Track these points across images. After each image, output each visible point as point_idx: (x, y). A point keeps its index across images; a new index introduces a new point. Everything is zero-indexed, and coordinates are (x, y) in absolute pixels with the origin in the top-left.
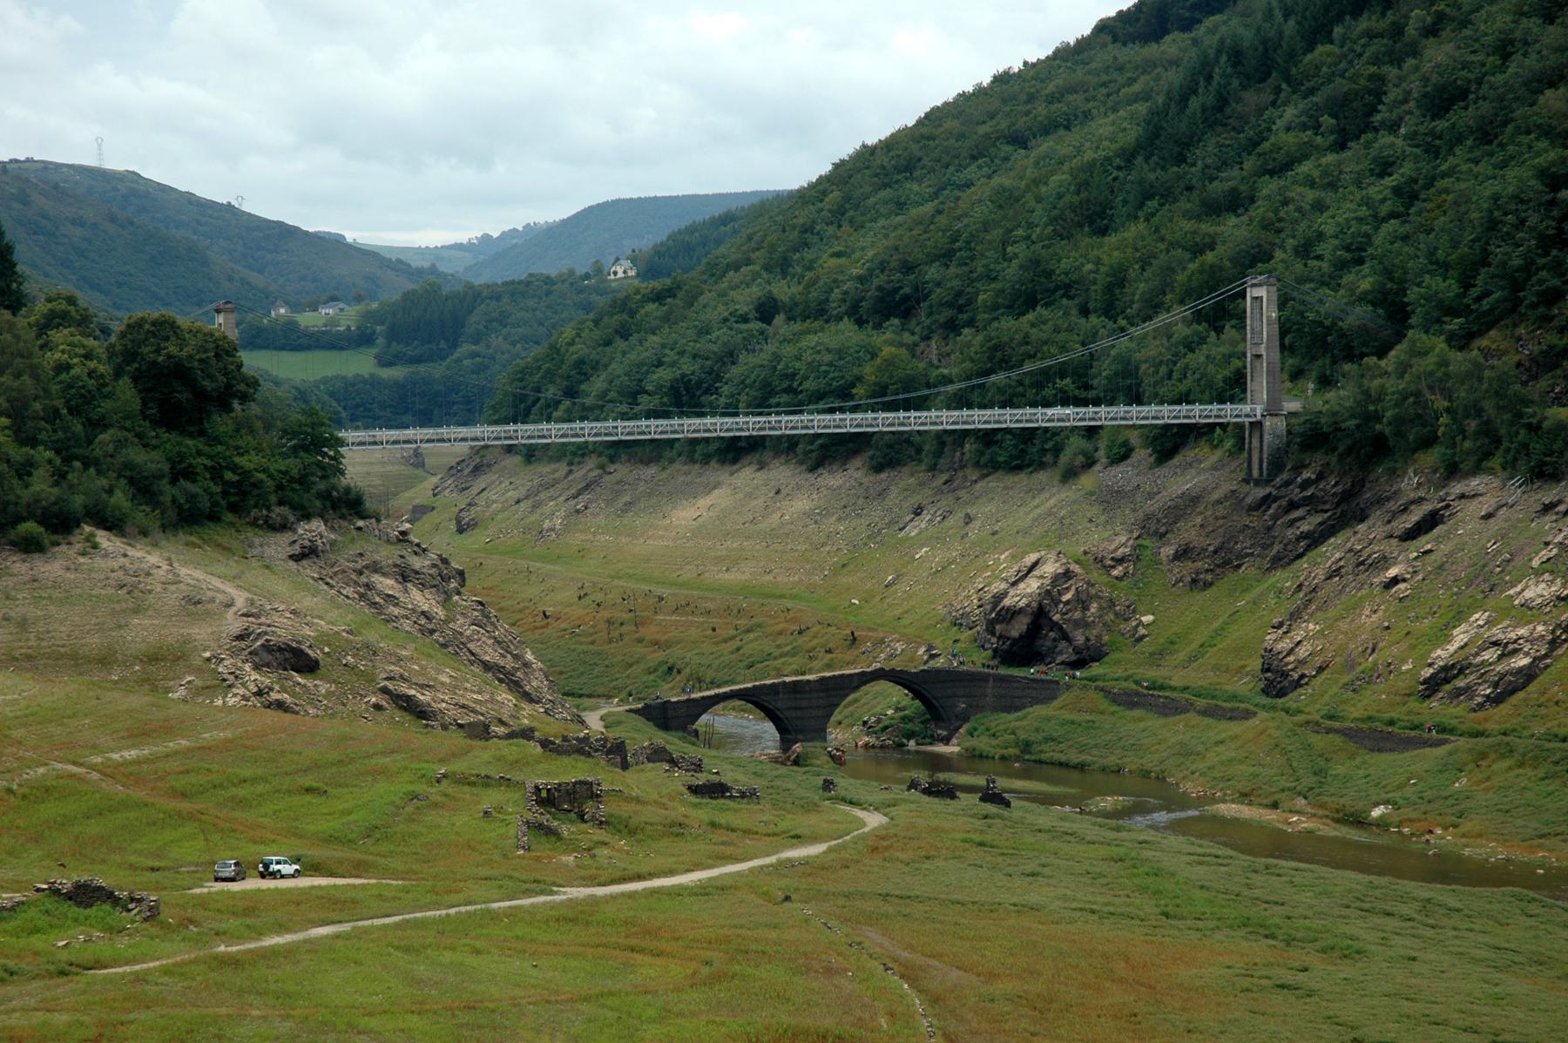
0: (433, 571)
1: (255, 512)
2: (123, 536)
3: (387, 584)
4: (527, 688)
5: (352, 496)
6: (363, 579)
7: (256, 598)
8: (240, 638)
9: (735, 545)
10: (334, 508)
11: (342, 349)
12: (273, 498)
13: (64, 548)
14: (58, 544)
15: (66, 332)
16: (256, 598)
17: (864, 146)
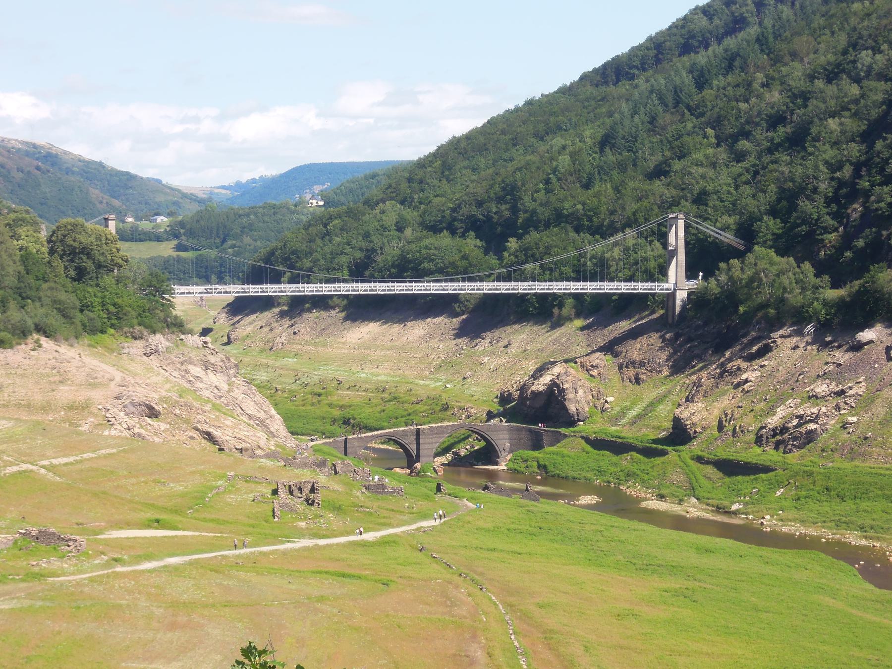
0: (221, 364)
1: (126, 329)
2: (56, 341)
3: (197, 370)
4: (272, 429)
5: (178, 321)
6: (184, 367)
7: (126, 376)
8: (117, 398)
9: (382, 353)
10: (168, 326)
11: (141, 240)
12: (135, 321)
13: (23, 346)
14: (20, 344)
15: (25, 229)
16: (126, 376)
17: (454, 137)
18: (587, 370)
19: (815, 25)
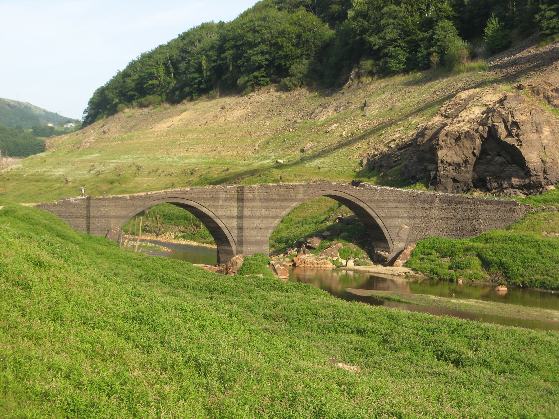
18: (547, 98)
19: (345, 167)
